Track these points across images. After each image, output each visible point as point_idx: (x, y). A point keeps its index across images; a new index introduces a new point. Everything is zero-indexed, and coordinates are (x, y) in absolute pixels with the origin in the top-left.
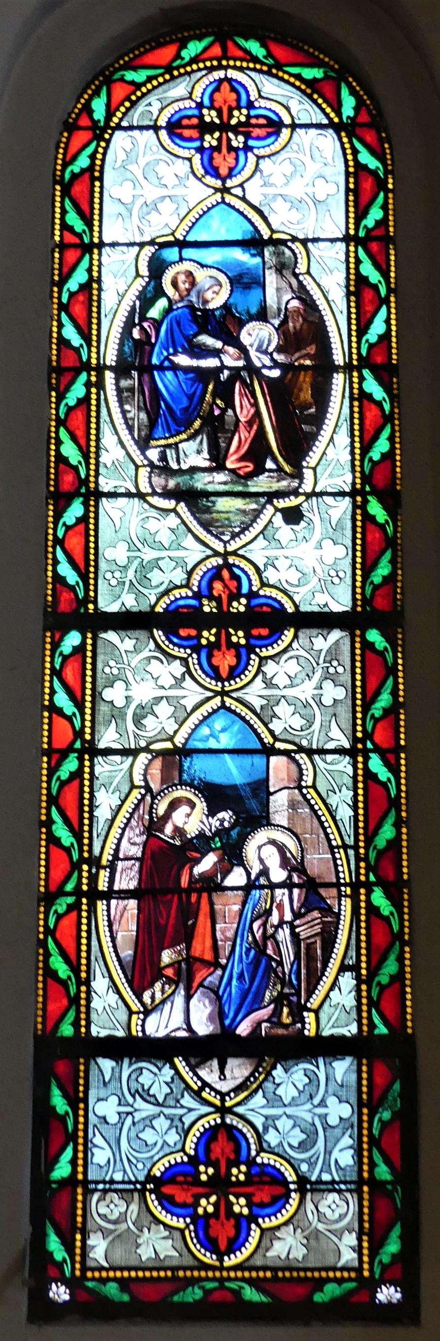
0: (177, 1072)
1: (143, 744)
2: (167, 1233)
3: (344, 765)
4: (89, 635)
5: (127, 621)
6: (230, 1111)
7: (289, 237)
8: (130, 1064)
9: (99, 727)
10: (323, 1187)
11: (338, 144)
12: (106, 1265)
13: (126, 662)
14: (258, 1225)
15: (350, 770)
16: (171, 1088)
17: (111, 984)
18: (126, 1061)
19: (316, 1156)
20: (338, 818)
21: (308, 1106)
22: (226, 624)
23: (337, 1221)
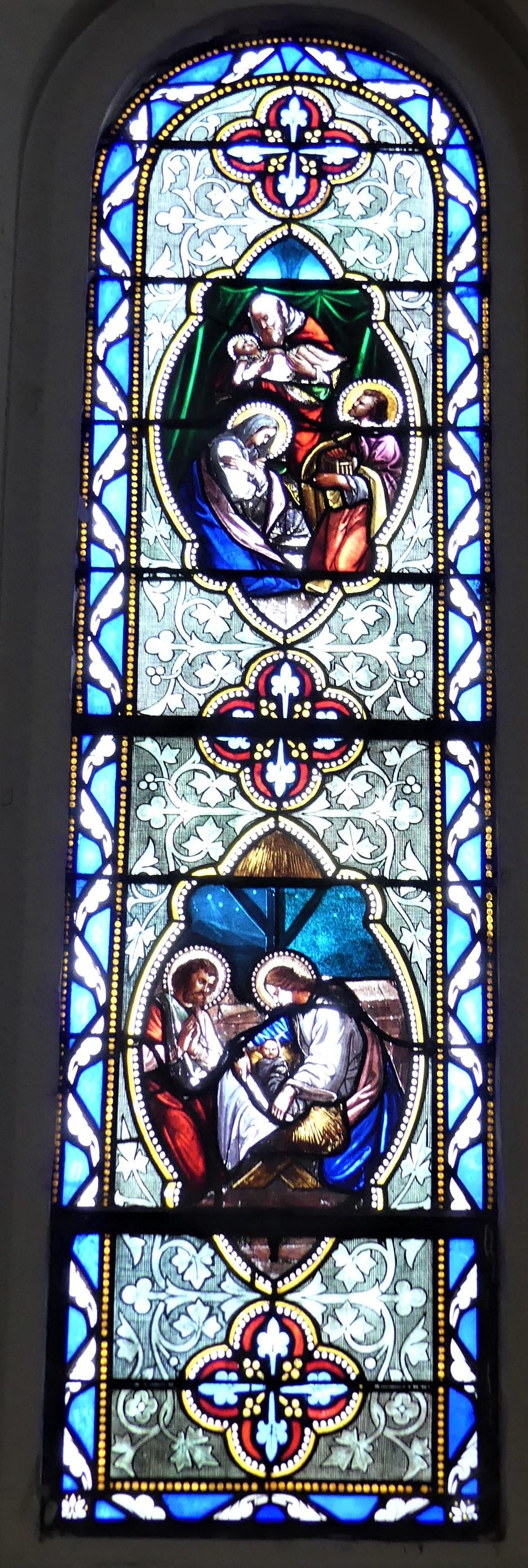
0: (217, 1252)
1: (184, 870)
2: (205, 1439)
3: (422, 901)
4: (125, 743)
5: (171, 727)
6: (281, 1297)
7: (365, 279)
8: (163, 1242)
9: (133, 852)
10: (392, 1387)
11: (426, 172)
12: (132, 1474)
13: (399, 684)
14: (312, 1429)
15: (427, 905)
16: (211, 1271)
17: (409, 352)
18: (391, 280)
19: (382, 1353)
20: (159, 509)
21: (376, 1291)
22: (265, 659)
23: (406, 1426)
